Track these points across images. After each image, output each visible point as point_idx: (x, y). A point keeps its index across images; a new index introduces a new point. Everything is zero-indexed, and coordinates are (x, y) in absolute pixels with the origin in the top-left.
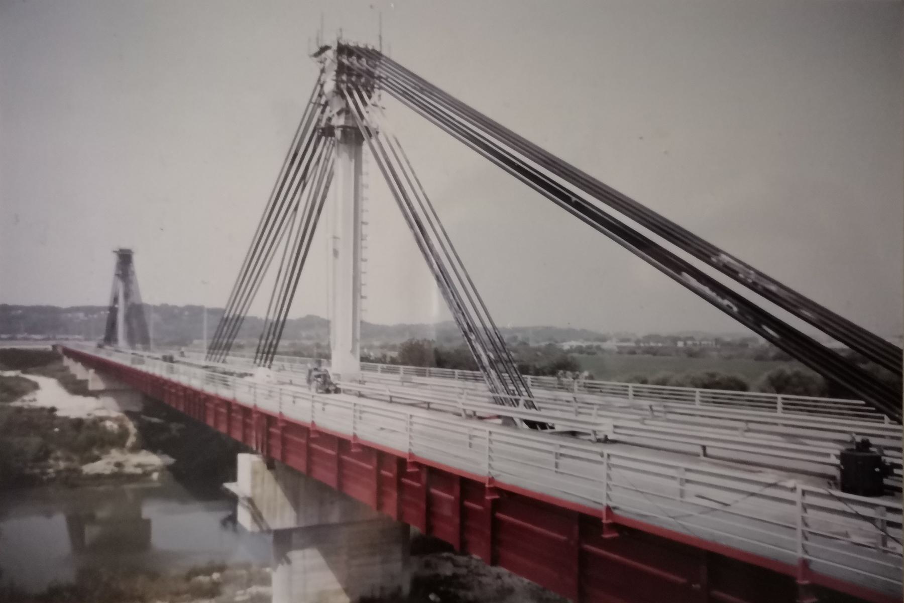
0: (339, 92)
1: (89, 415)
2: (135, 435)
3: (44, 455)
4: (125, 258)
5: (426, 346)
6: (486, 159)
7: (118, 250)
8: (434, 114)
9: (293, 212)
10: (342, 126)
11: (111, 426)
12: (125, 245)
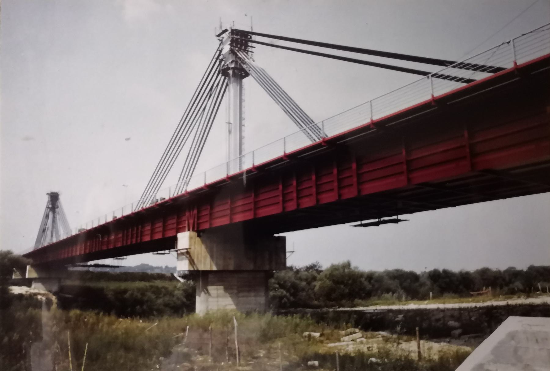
0: (232, 52)
1: (27, 292)
2: (57, 303)
4: (54, 198)
7: (50, 193)
8: (272, 95)
9: (202, 111)
10: (232, 68)
11: (41, 298)
12: (55, 190)
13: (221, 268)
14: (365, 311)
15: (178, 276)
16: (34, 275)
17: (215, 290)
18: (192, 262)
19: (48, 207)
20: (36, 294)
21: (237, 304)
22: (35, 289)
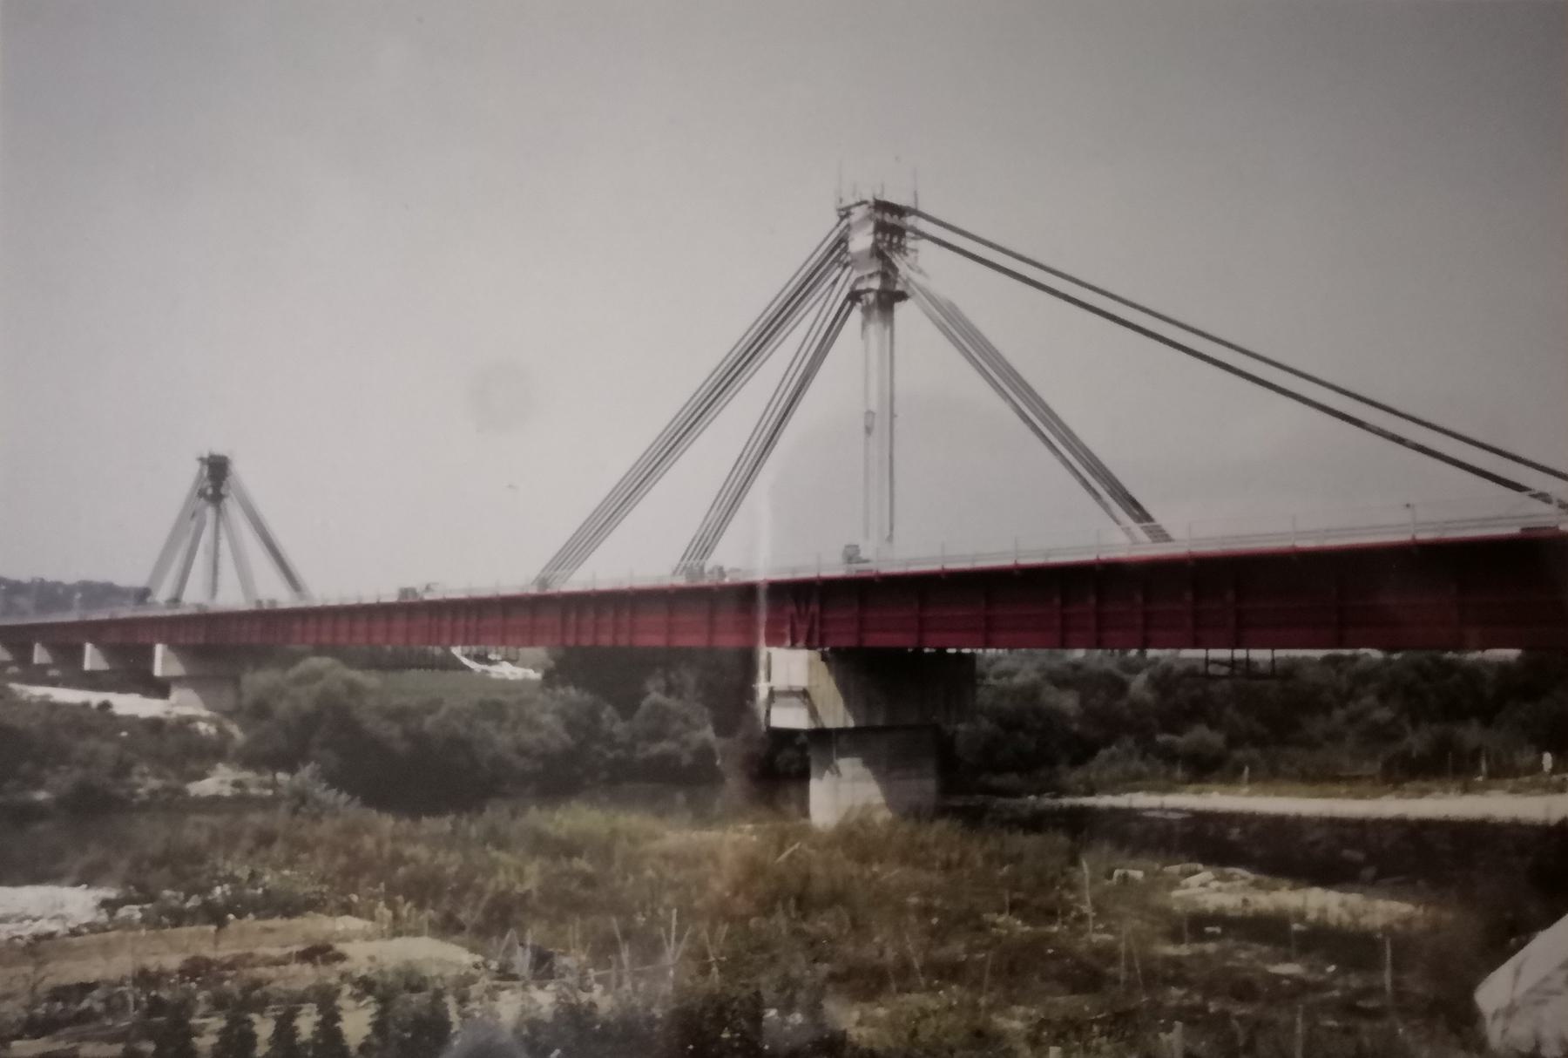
3: (122, 770)
4: (217, 469)
5: (1441, 794)
6: (847, 322)
7: (206, 455)
11: (207, 730)
12: (219, 450)
13: (862, 723)
14: (1144, 814)
15: (462, 655)
16: (177, 669)
17: (849, 766)
18: (813, 713)
19: (202, 494)
20: (191, 719)
21: (887, 793)
22: (179, 704)
